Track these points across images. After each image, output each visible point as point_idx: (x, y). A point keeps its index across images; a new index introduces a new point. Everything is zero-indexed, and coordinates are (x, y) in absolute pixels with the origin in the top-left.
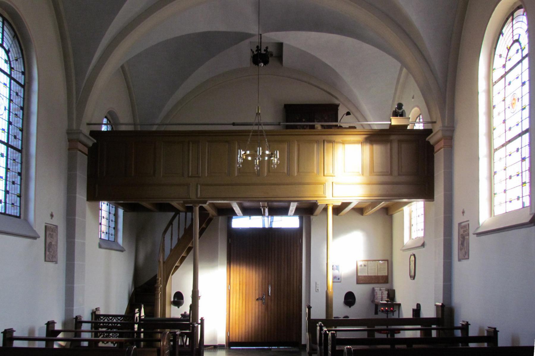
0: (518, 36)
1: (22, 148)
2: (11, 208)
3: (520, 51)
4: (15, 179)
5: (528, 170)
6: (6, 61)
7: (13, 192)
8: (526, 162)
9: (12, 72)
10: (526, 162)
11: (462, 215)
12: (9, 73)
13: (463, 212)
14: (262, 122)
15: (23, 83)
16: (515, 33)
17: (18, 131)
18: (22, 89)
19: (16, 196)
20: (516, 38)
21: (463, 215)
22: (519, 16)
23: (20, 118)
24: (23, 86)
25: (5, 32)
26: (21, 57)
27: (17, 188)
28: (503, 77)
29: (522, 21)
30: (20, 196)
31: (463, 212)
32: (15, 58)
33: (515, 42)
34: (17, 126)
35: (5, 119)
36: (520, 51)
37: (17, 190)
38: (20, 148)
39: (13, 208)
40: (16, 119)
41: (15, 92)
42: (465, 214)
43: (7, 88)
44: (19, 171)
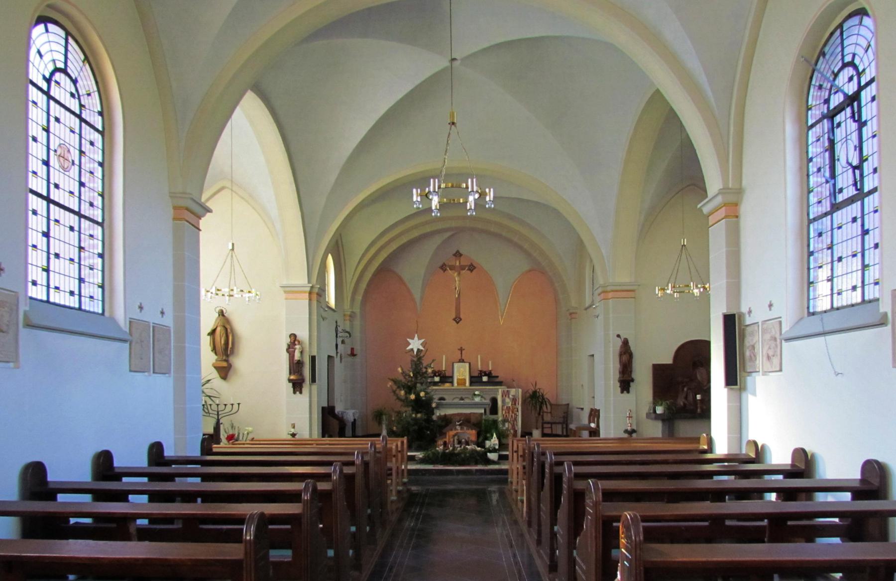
0: (851, 56)
1: (103, 219)
2: (90, 303)
3: (855, 78)
4: (94, 184)
5: (861, 235)
6: (72, 95)
7: (91, 281)
8: (857, 259)
9: (83, 111)
10: (857, 259)
11: (768, 309)
12: (78, 112)
13: (770, 305)
14: (485, 420)
15: (100, 128)
16: (846, 51)
17: (96, 165)
18: (100, 137)
19: (96, 286)
20: (848, 59)
21: (770, 310)
22: (850, 37)
23: (98, 240)
24: (102, 133)
25: (69, 45)
26: (96, 91)
27: (98, 245)
28: (829, 215)
29: (858, 35)
30: (101, 256)
31: (770, 305)
32: (86, 91)
33: (845, 65)
34: (94, 281)
35: (73, 244)
36: (855, 78)
37: (98, 279)
38: (100, 220)
39: (92, 303)
40: (91, 241)
41: (88, 201)
42: (772, 308)
43: (76, 198)
44: (100, 160)
